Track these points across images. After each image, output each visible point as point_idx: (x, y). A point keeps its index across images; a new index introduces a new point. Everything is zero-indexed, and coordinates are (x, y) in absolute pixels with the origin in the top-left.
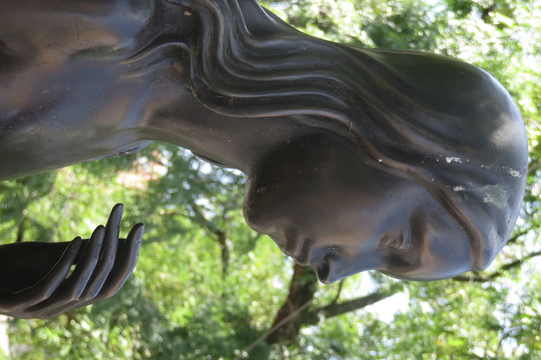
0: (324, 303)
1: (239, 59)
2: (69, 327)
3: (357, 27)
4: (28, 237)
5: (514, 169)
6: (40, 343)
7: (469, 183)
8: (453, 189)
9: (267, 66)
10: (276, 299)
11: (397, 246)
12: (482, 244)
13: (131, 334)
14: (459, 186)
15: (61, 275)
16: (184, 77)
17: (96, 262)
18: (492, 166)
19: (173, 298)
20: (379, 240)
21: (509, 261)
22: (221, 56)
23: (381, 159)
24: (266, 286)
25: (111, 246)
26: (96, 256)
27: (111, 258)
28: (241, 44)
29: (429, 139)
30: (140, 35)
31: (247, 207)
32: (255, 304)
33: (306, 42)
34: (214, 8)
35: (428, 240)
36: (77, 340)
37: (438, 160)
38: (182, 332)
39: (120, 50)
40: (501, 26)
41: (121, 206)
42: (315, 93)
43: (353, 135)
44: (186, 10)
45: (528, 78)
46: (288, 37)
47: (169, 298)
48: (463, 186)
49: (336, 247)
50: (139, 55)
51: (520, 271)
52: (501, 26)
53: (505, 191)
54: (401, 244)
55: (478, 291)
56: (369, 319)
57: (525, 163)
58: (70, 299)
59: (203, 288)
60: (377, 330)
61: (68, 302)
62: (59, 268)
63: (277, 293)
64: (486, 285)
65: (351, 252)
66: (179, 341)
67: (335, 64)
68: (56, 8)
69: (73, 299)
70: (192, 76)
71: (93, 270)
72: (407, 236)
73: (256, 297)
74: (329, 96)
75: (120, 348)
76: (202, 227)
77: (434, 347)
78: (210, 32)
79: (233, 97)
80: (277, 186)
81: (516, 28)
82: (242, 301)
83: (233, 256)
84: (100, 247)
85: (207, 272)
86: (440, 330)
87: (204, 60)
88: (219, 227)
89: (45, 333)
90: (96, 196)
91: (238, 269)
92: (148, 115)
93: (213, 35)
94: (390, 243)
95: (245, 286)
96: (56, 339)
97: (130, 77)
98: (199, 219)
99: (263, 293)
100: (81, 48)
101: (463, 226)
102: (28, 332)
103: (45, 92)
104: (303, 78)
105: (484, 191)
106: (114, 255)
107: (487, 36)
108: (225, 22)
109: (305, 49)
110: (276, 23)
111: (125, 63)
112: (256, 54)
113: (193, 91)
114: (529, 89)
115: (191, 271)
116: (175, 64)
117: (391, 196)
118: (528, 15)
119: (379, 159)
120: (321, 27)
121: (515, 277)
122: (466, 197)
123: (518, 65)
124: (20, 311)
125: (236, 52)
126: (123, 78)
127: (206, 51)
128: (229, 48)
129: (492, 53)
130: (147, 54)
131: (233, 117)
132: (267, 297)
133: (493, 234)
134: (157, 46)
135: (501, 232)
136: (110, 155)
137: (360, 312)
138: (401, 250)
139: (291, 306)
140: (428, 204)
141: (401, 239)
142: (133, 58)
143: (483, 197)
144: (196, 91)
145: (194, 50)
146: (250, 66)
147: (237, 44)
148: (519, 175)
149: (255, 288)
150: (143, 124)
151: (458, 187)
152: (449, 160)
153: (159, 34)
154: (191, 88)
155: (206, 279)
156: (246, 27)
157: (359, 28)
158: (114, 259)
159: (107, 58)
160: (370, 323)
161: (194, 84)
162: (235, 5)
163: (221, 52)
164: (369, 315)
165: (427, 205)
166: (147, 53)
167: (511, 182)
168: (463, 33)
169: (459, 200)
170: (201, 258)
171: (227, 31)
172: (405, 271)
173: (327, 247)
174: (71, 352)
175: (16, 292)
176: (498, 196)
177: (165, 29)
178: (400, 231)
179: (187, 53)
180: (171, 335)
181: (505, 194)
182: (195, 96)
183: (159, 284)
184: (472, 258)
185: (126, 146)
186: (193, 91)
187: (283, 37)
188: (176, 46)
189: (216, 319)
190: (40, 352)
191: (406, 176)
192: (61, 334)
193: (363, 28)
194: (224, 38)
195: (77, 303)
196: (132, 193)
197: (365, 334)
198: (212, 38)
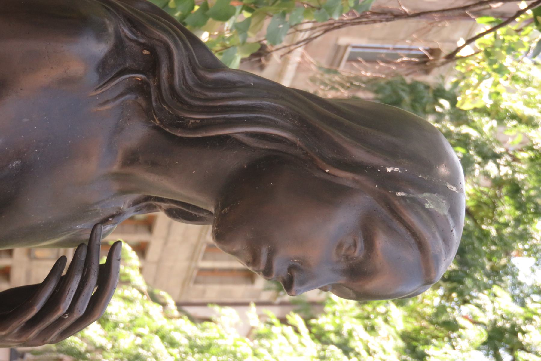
7: (410, 189)
9: (220, 94)
23: (328, 170)
25: (93, 262)
43: (301, 152)
48: (405, 192)
53: (444, 201)
57: (461, 183)
58: (58, 309)
71: (78, 283)
92: (119, 157)
93: (169, 66)
101: (410, 232)
109: (253, 84)
113: (156, 119)
119: (326, 169)
122: (408, 201)
125: (190, 82)
141: (355, 245)
142: (101, 89)
144: (158, 118)
145: (154, 81)
146: (204, 95)
150: (115, 168)
166: (112, 83)
167: (449, 194)
181: (444, 204)
198: (168, 69)
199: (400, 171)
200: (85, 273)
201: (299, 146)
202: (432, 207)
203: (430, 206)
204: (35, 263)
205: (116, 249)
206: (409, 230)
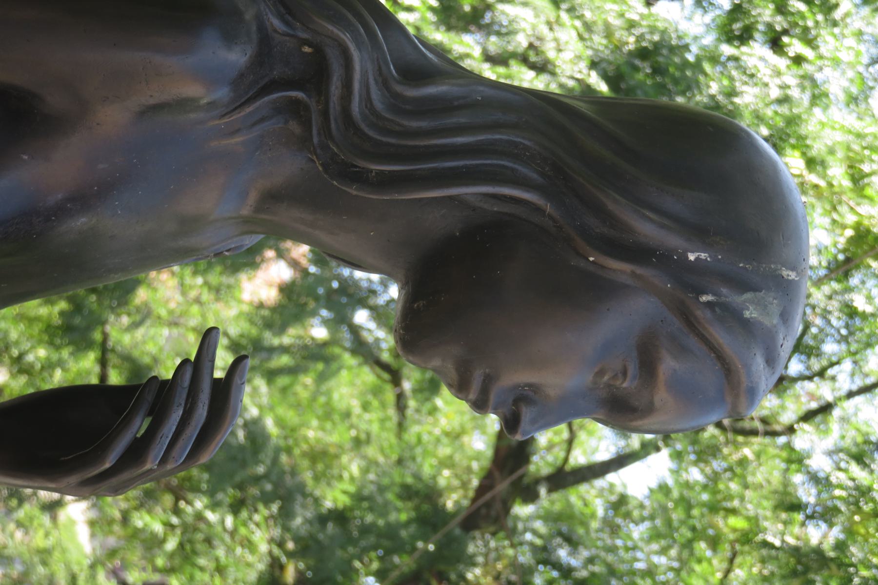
0: (546, 471)
1: (382, 113)
2: (177, 511)
3: (583, 65)
4: (115, 378)
5: (787, 269)
6: (136, 534)
8: (698, 299)
9: (423, 124)
10: (475, 465)
11: (618, 383)
12: (744, 379)
14: (707, 294)
15: (130, 432)
16: (304, 142)
17: (181, 412)
18: (755, 264)
19: (826, 500)
20: (593, 375)
21: (814, 405)
22: (357, 109)
24: (462, 447)
26: (181, 404)
27: (202, 406)
28: (386, 92)
29: (662, 226)
30: (238, 81)
31: (399, 330)
32: (446, 473)
33: (481, 88)
34: (344, 40)
35: (664, 374)
36: (188, 529)
37: (675, 257)
38: (340, 517)
39: (209, 104)
40: (798, 60)
41: (216, 331)
42: (495, 162)
44: (305, 44)
45: (839, 137)
46: (454, 81)
47: (320, 467)
48: (714, 294)
49: (530, 385)
50: (237, 111)
51: (831, 419)
54: (625, 379)
55: (772, 451)
57: (804, 260)
58: (144, 466)
59: (371, 451)
60: (623, 509)
61: (140, 471)
62: (127, 422)
63: (478, 456)
64: (782, 440)
65: (552, 392)
67: (524, 120)
68: (115, 45)
69: (148, 466)
70: (315, 140)
71: (176, 424)
72: (632, 369)
73: (447, 463)
74: (516, 166)
75: (251, 540)
78: (340, 75)
79: (375, 170)
80: (443, 299)
81: (819, 63)
82: (427, 470)
83: (412, 403)
84: (186, 391)
85: (375, 428)
86: (713, 508)
87: (332, 117)
89: (141, 518)
91: (419, 422)
92: (253, 198)
94: (609, 379)
96: (158, 528)
97: (226, 142)
99: (457, 457)
100: (152, 101)
101: (715, 353)
102: (117, 519)
103: (101, 166)
104: (477, 141)
105: (745, 302)
106: (207, 402)
107: (778, 73)
108: (361, 61)
109: (480, 98)
110: (436, 60)
111: (217, 122)
112: (408, 107)
113: (317, 163)
114: (840, 154)
116: (291, 123)
117: (608, 310)
118: (838, 44)
120: (533, 67)
122: (717, 309)
124: (72, 485)
125: (378, 105)
126: (214, 144)
127: (335, 104)
128: (367, 99)
131: (377, 199)
132: (465, 463)
133: (759, 362)
134: (263, 98)
136: (200, 257)
137: (599, 483)
138: (625, 388)
139: (497, 474)
140: (662, 321)
141: (625, 373)
143: (743, 309)
145: (318, 102)
146: (399, 125)
147: (379, 93)
148: (796, 277)
149: (445, 451)
150: (246, 211)
151: (705, 295)
152: (692, 257)
153: (266, 80)
154: (314, 158)
156: (392, 67)
157: (587, 66)
158: (206, 408)
159: (192, 116)
160: (614, 498)
161: (319, 151)
162: (376, 36)
163: (357, 105)
164: (612, 486)
165: (660, 323)
169: (708, 314)
170: (366, 407)
171: (364, 74)
172: (631, 421)
173: (516, 387)
174: (181, 545)
175: (66, 458)
176: (763, 307)
177: (275, 73)
178: (623, 361)
179: (307, 108)
180: (323, 519)
182: (320, 168)
183: (305, 447)
184: (729, 399)
185: (223, 244)
186: (317, 163)
187: (447, 81)
188: (291, 97)
189: (390, 496)
190: (135, 547)
191: (629, 281)
192: (165, 520)
193: (594, 65)
194: (360, 83)
195: (155, 472)
197: (606, 514)
199: (709, 259)
200: (189, 405)
201: (549, 215)
202: (756, 316)
203: (752, 314)
204: (76, 568)
205: (239, 369)
206: (712, 349)
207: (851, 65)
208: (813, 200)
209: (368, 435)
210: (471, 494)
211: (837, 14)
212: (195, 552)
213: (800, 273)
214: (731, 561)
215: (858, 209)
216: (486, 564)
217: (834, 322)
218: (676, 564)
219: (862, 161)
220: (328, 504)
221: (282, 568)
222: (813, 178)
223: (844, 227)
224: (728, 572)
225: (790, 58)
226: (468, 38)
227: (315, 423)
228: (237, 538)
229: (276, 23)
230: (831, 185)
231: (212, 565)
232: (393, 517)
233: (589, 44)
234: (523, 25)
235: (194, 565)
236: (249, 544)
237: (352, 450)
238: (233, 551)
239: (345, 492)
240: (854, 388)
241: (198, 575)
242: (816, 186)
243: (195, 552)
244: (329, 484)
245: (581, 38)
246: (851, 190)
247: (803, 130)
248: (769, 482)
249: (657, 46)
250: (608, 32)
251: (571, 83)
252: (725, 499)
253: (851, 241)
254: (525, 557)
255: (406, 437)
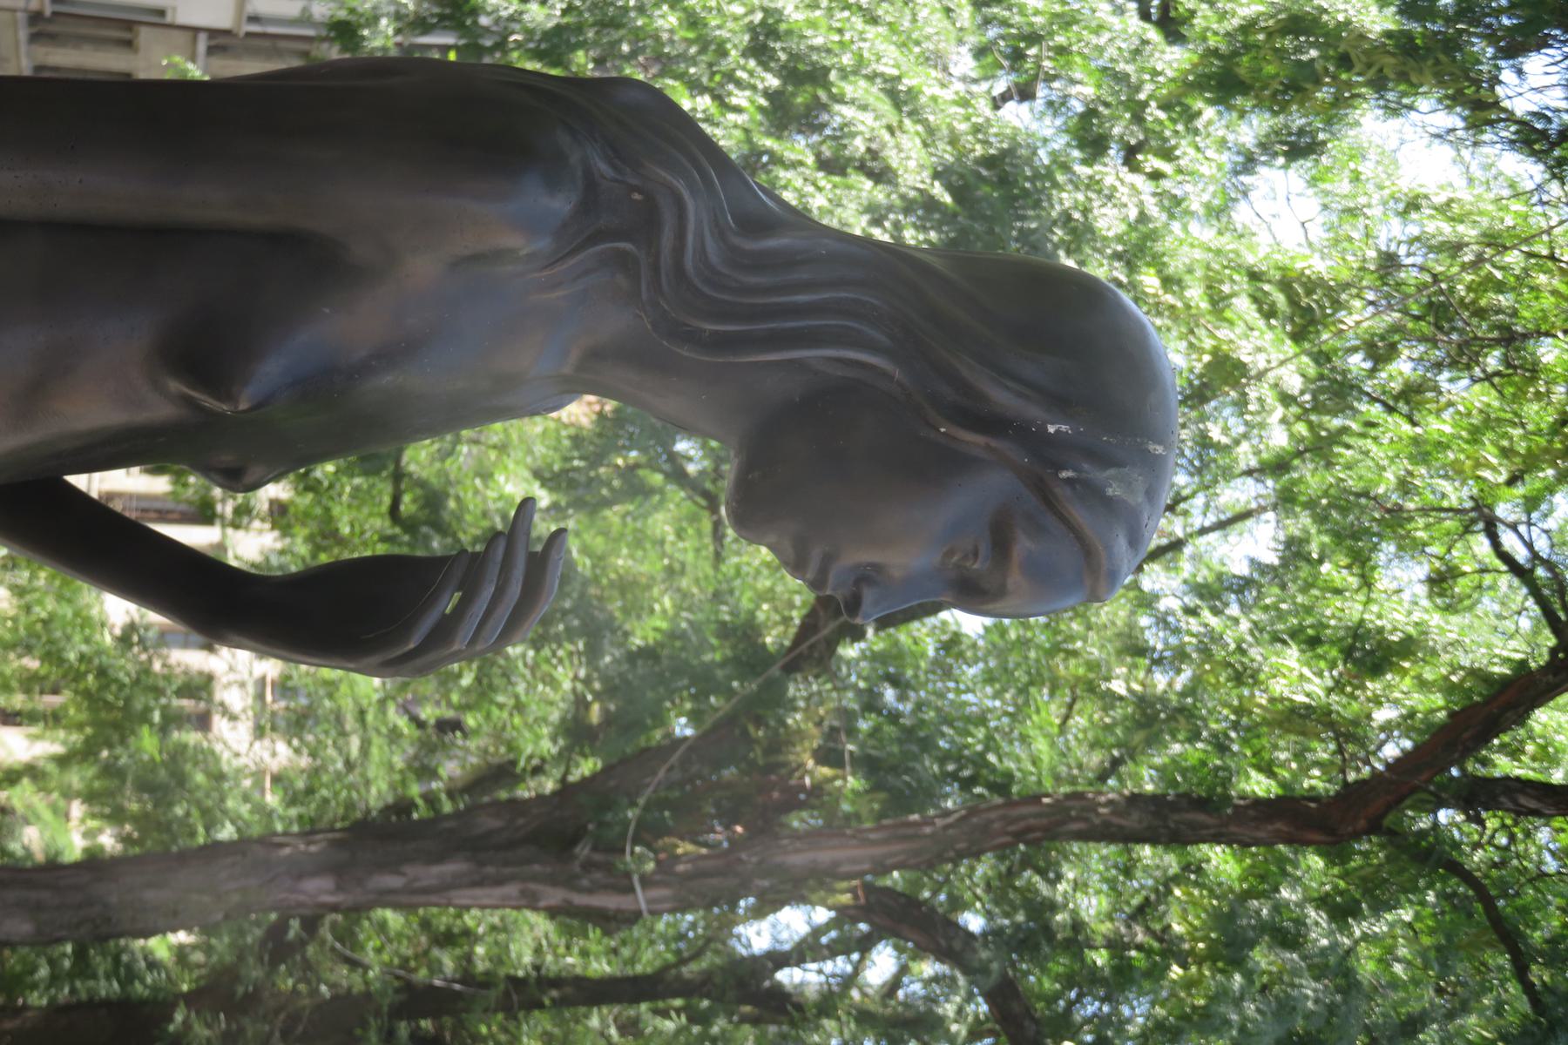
3: (926, 174)
13: (571, 654)
29: (1020, 395)
40: (1156, 176)
45: (1198, 254)
48: (1075, 470)
52: (1156, 176)
56: (944, 632)
59: (684, 583)
60: (956, 650)
62: (433, 599)
65: (897, 573)
66: (642, 668)
69: (456, 647)
70: (644, 296)
72: (984, 549)
76: (682, 486)
77: (1046, 674)
81: (1180, 178)
86: (1055, 649)
88: (708, 485)
90: (515, 436)
91: (738, 553)
95: (750, 580)
98: (677, 475)
107: (1134, 190)
114: (1199, 273)
115: (664, 555)
121: (1172, 568)
123: (1182, 235)
129: (1143, 217)
130: (572, 262)
133: (1121, 544)
135: (1135, 540)
141: (976, 555)
150: (567, 370)
152: (1051, 429)
155: (689, 568)
160: (945, 638)
162: (712, 182)
164: (944, 623)
168: (1093, 184)
170: (680, 534)
171: (700, 236)
180: (633, 657)
193: (936, 175)
196: (572, 431)
204: (365, 702)
207: (1212, 179)
208: (1168, 322)
209: (683, 565)
210: (793, 631)
211: (1199, 123)
212: (491, 687)
213: (1168, 447)
214: (1070, 707)
215: (1218, 333)
216: (806, 710)
217: (1187, 452)
218: (1011, 709)
219: (1221, 282)
220: (637, 641)
221: (587, 706)
222: (1169, 299)
223: (1201, 351)
224: (1066, 718)
225: (1249, 473)
226: (801, 141)
227: (625, 551)
228: (538, 675)
229: (603, 167)
230: (1188, 307)
231: (512, 702)
232: (707, 657)
233: (932, 150)
234: (861, 128)
235: (492, 702)
236: (552, 682)
237: (664, 581)
238: (535, 687)
239: (656, 629)
240: (1207, 523)
241: (495, 712)
242: (1172, 307)
243: (491, 687)
244: (639, 617)
245: (925, 145)
246: (1210, 312)
247: (1159, 247)
248: (1114, 623)
249: (1004, 154)
250: (954, 140)
251: (912, 194)
252: (1065, 641)
253: (1208, 365)
254: (850, 701)
255: (724, 568)
